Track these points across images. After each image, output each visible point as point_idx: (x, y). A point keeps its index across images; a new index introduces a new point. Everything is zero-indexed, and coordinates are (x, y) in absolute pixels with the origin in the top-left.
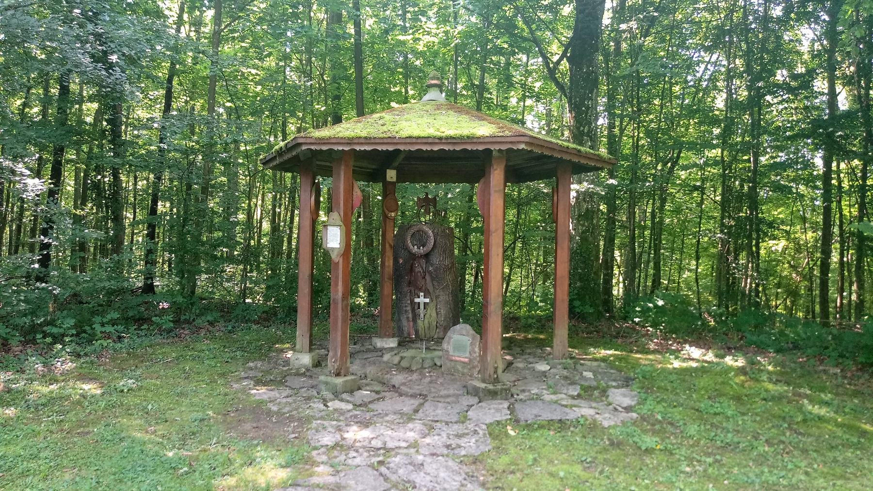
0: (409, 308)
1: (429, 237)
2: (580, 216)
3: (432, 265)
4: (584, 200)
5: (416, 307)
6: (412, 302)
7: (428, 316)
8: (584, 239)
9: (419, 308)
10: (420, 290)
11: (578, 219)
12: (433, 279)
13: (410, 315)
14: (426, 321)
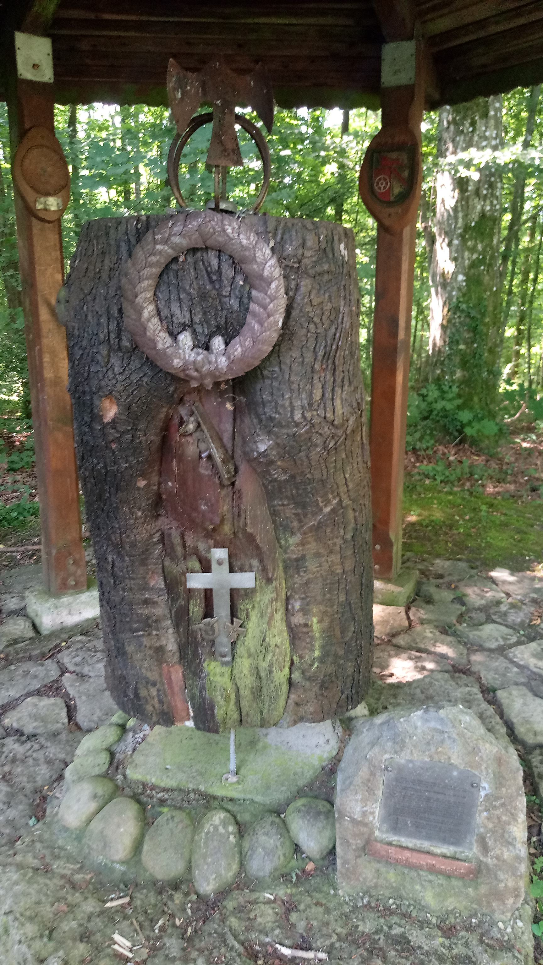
0: (161, 609)
1: (253, 281)
2: (467, 228)
3: (269, 426)
4: (477, 192)
5: (196, 610)
6: (174, 585)
7: (250, 640)
8: (474, 280)
9: (208, 613)
10: (213, 536)
11: (462, 236)
12: (271, 492)
13: (170, 643)
14: (244, 665)
